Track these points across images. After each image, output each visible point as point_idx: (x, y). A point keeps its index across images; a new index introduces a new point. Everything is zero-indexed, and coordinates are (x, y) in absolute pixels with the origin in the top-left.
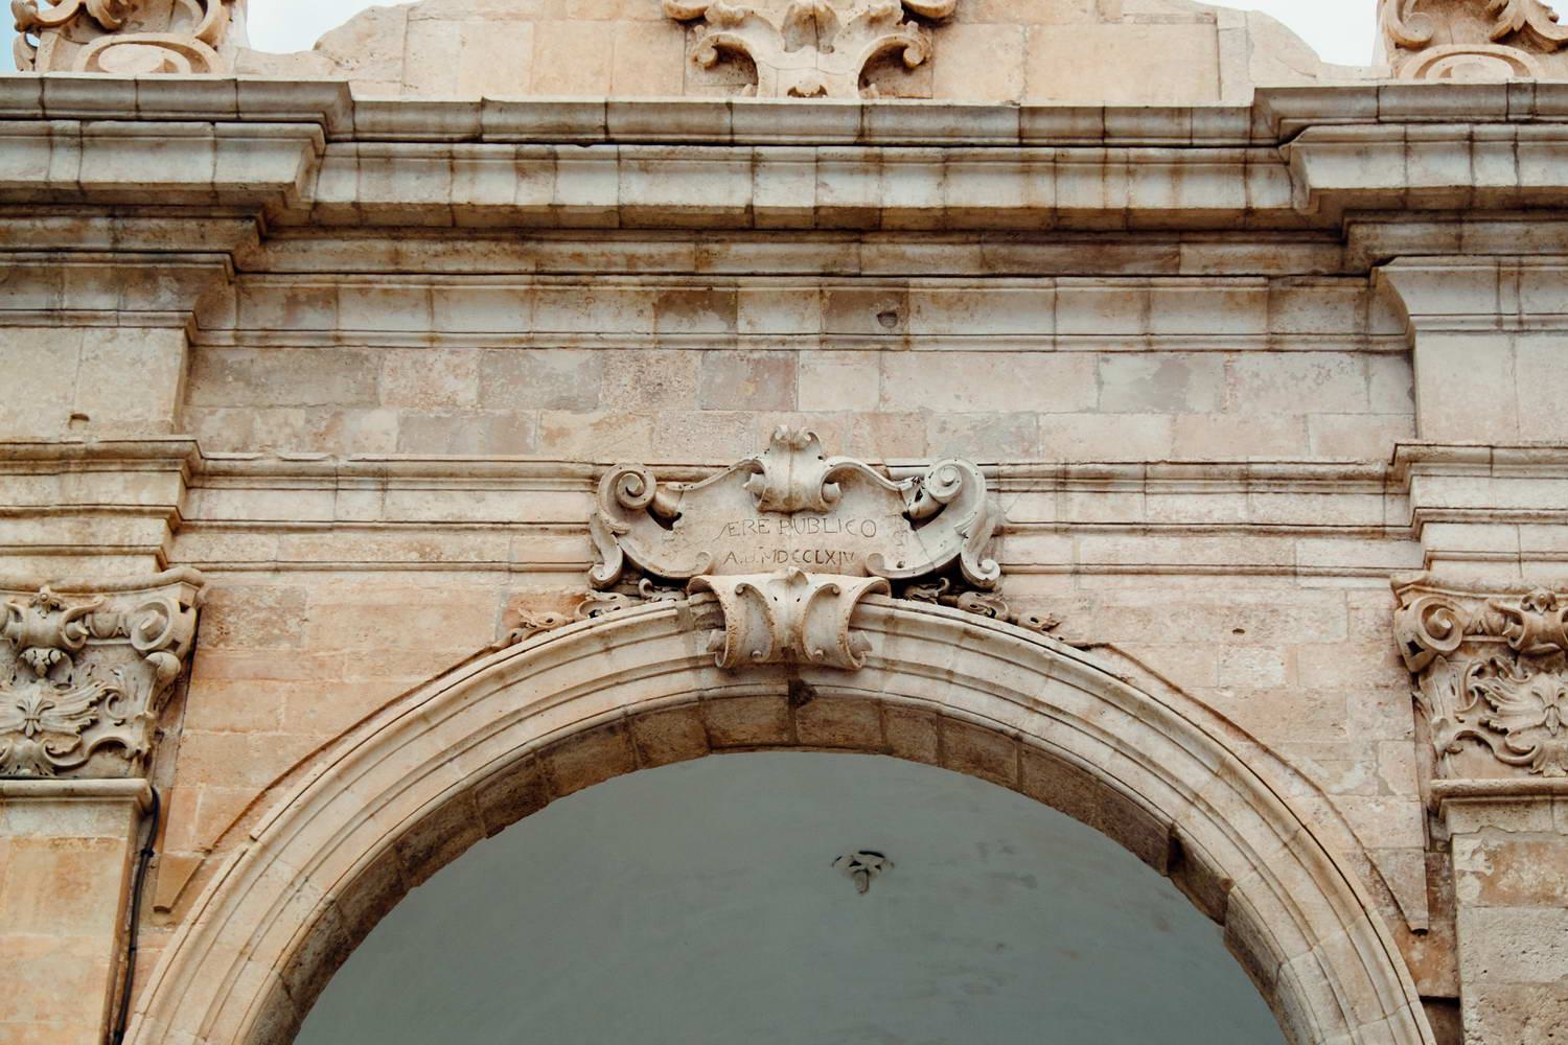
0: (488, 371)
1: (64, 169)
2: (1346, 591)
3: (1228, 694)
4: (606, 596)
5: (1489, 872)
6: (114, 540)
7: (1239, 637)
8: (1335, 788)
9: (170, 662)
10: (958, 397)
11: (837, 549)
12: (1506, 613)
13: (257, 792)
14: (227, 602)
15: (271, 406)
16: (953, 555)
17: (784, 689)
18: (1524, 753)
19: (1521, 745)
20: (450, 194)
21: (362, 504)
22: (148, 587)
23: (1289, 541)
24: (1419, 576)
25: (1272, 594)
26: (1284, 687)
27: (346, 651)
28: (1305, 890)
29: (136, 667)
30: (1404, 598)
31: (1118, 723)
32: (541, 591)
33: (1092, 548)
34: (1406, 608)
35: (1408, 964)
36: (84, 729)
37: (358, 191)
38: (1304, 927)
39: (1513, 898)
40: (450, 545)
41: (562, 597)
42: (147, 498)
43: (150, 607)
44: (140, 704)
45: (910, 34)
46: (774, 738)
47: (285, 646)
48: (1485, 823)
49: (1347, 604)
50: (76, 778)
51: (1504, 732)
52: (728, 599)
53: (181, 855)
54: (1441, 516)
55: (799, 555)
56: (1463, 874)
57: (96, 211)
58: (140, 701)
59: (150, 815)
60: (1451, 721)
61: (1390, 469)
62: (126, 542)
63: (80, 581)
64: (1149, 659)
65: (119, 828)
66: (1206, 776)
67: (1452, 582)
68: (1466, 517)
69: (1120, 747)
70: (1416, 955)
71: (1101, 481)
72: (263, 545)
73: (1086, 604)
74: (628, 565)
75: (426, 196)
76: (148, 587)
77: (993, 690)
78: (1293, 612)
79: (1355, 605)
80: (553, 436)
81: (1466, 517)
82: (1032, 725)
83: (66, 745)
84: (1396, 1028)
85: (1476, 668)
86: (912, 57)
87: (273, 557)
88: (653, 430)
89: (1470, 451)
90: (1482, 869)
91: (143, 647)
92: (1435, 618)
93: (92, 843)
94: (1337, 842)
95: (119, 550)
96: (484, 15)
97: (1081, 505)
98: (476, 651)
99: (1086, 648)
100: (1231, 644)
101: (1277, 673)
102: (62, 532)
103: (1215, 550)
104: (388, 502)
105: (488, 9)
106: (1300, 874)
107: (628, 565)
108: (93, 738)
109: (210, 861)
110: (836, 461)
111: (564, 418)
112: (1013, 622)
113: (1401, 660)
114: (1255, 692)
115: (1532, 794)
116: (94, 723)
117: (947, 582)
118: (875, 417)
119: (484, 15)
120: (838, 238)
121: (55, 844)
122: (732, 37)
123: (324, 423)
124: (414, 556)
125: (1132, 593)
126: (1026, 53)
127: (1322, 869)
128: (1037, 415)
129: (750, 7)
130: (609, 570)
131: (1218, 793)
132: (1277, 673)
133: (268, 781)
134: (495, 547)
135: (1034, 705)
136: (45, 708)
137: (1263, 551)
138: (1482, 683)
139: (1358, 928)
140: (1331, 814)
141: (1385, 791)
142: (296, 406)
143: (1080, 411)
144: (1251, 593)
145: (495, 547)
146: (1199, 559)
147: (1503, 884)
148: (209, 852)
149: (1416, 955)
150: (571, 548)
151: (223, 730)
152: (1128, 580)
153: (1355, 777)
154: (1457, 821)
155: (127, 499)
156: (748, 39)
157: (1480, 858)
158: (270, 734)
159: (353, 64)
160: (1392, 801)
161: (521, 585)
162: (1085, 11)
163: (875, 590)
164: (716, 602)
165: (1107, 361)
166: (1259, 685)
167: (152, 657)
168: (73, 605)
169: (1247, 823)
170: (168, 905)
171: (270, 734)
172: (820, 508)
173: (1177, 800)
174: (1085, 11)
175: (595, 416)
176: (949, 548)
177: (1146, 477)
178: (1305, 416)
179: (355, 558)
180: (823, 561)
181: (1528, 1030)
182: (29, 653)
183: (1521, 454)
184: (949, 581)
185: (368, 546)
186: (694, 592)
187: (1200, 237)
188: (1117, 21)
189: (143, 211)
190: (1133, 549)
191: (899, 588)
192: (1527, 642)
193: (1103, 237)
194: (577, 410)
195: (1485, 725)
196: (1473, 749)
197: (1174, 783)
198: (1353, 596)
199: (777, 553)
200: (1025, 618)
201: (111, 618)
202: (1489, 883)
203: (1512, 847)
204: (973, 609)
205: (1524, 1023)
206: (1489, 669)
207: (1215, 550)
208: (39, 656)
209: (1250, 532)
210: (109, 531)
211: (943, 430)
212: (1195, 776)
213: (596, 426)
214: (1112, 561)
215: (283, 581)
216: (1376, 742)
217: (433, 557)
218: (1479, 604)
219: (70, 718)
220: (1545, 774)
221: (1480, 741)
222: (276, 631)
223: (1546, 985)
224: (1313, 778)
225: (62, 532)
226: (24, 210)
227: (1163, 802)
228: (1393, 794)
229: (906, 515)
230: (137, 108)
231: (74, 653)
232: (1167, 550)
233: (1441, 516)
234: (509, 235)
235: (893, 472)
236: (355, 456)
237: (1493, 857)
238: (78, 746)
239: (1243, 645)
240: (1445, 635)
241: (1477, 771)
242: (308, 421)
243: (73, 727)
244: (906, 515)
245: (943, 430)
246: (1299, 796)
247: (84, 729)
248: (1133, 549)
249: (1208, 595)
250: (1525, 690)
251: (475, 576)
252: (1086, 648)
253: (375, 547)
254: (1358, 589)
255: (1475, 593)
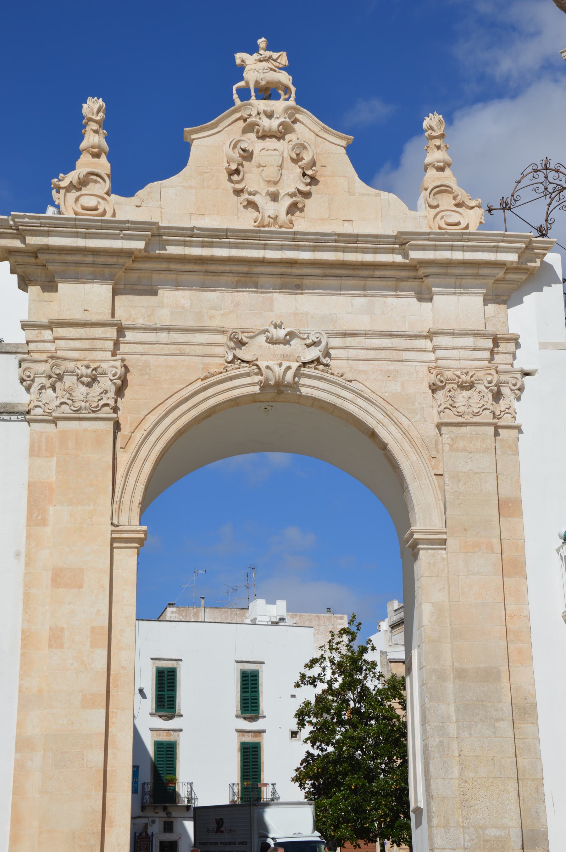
0: (192, 298)
1: (81, 243)
2: (415, 366)
3: (387, 394)
4: (230, 365)
5: (451, 443)
6: (100, 347)
7: (389, 378)
8: (413, 420)
9: (119, 382)
10: (316, 309)
11: (289, 354)
12: (457, 376)
13: (143, 417)
14: (130, 364)
15: (135, 307)
16: (318, 356)
17: (276, 391)
18: (460, 413)
19: (459, 410)
20: (184, 251)
21: (163, 337)
22: (111, 361)
23: (402, 352)
24: (435, 365)
25: (397, 366)
26: (400, 392)
27: (163, 378)
28: (407, 446)
29: (110, 383)
30: (431, 371)
31: (360, 401)
32: (211, 362)
33: (352, 353)
34: (432, 373)
35: (431, 465)
36: (99, 400)
37: (463, 553)
38: (406, 455)
39: (457, 450)
40: (187, 349)
41: (217, 364)
42: (108, 336)
43: (112, 367)
44: (112, 394)
45: (299, 198)
46: (270, 400)
47: (147, 377)
48: (450, 430)
49: (416, 369)
50: (98, 414)
51: (455, 407)
52: (263, 369)
53: (125, 433)
54: (440, 348)
55: (279, 355)
56: (445, 444)
57: (89, 253)
58: (112, 393)
59: (117, 426)
60: (443, 404)
61: (428, 334)
62: (104, 348)
63: (92, 358)
64: (367, 384)
65: (110, 426)
66: (382, 417)
67: (443, 366)
68: (446, 348)
69: (360, 407)
70: (433, 463)
71: (354, 335)
72: (138, 348)
73: (350, 368)
74: (235, 357)
75: (178, 252)
76: (111, 361)
77: (328, 392)
78: (402, 372)
79: (418, 370)
80: (211, 317)
81: (446, 348)
82: (338, 402)
83: (95, 405)
84: (428, 482)
85: (449, 390)
86: (300, 206)
87: (141, 351)
88: (237, 316)
89: (448, 331)
90: (450, 443)
91: (112, 378)
92: (439, 376)
93: (104, 431)
94: (414, 433)
95: (102, 350)
96: (182, 187)
97: (349, 341)
98: (196, 379)
99: (350, 381)
100: (387, 380)
101: (399, 389)
102: (86, 344)
103: (383, 354)
104: (170, 337)
105: (182, 185)
106: (405, 442)
107: (235, 357)
108: (101, 403)
109: (133, 435)
110: (288, 330)
111: (214, 312)
112: (332, 374)
113: (430, 386)
114: (393, 394)
115: (462, 424)
116: (102, 399)
117: (316, 362)
118: (295, 314)
119: (182, 187)
120: (286, 265)
121: (95, 431)
122: (252, 198)
123: (150, 312)
124: (178, 352)
125: (362, 366)
126: (329, 204)
127: (411, 441)
128: (336, 314)
129: (256, 189)
130: (230, 358)
131: (386, 421)
132: (399, 389)
133: (146, 414)
134: (199, 350)
135: (339, 396)
136: (88, 394)
137: (395, 355)
138: (450, 394)
139: (420, 457)
140: (412, 426)
141: (426, 421)
142: (142, 307)
143: (347, 313)
144: (392, 366)
145: (199, 350)
146: (379, 357)
147: (454, 446)
148: (133, 433)
149: (433, 463)
150: (220, 350)
151: (133, 399)
152: (361, 362)
153: (418, 417)
154: (444, 429)
155: (103, 336)
156: (256, 199)
157: (449, 440)
158: (145, 401)
159: (147, 201)
160: (427, 423)
161: (207, 360)
162: (345, 191)
163: (300, 366)
164: (259, 368)
165: (354, 299)
166: (394, 392)
167: (114, 381)
168: (93, 366)
169: (393, 428)
170: (124, 447)
171: (145, 401)
172: (286, 342)
173: (375, 422)
174: (345, 191)
175: (222, 312)
176: (317, 354)
177: (365, 335)
178: (405, 316)
179: (163, 352)
180: (287, 358)
181: (460, 483)
182: (82, 379)
183: (461, 332)
184: (317, 361)
185: (166, 349)
186: (253, 365)
187: (380, 268)
188: (354, 195)
189: (102, 254)
190: (362, 354)
191: (304, 364)
192: (462, 384)
193: (355, 267)
194: (217, 310)
195: (451, 405)
196: (447, 410)
197: (374, 418)
198: (417, 368)
199: (273, 355)
200: (336, 373)
201: (102, 369)
202: (451, 446)
203: (457, 437)
204: (323, 371)
205: (459, 482)
206: (452, 390)
207: (383, 354)
208: (86, 380)
209: (392, 350)
210: (99, 344)
211: (312, 318)
212: (380, 416)
213: (222, 315)
214: (357, 357)
215: (144, 357)
216: (423, 408)
217: (183, 352)
218: (449, 372)
219: (95, 397)
220: (465, 418)
221: (449, 409)
222: (144, 372)
223: (464, 472)
224: (408, 417)
225: (86, 344)
226: (69, 252)
227: (371, 423)
228: (427, 421)
229: (306, 344)
230: (101, 227)
231: (94, 379)
232: (371, 354)
233: (440, 348)
234: (199, 262)
235: (301, 332)
236: (161, 324)
237: (452, 439)
238: (98, 405)
239: (390, 381)
240: (442, 382)
241: (450, 417)
242: (146, 311)
243: (96, 399)
244: (306, 344)
245: (312, 318)
246: (404, 421)
247: (99, 400)
248: (362, 354)
249: (381, 367)
250: (460, 396)
251: (194, 357)
252: (350, 381)
253: (167, 349)
254: (418, 366)
255: (448, 369)
